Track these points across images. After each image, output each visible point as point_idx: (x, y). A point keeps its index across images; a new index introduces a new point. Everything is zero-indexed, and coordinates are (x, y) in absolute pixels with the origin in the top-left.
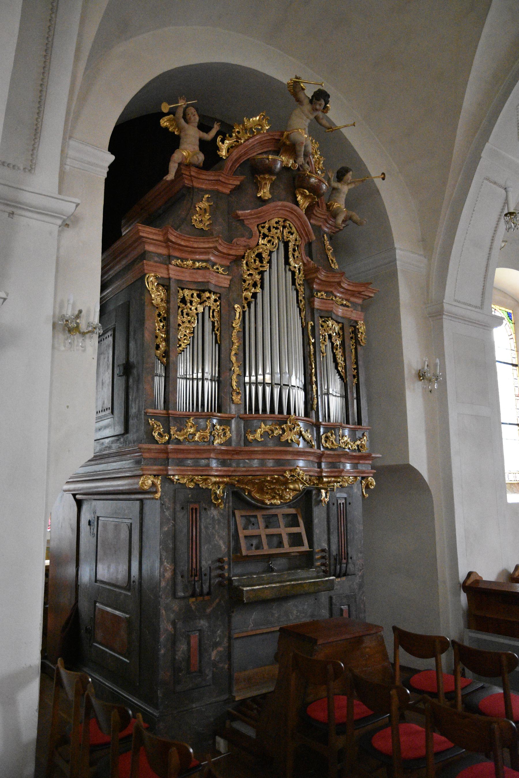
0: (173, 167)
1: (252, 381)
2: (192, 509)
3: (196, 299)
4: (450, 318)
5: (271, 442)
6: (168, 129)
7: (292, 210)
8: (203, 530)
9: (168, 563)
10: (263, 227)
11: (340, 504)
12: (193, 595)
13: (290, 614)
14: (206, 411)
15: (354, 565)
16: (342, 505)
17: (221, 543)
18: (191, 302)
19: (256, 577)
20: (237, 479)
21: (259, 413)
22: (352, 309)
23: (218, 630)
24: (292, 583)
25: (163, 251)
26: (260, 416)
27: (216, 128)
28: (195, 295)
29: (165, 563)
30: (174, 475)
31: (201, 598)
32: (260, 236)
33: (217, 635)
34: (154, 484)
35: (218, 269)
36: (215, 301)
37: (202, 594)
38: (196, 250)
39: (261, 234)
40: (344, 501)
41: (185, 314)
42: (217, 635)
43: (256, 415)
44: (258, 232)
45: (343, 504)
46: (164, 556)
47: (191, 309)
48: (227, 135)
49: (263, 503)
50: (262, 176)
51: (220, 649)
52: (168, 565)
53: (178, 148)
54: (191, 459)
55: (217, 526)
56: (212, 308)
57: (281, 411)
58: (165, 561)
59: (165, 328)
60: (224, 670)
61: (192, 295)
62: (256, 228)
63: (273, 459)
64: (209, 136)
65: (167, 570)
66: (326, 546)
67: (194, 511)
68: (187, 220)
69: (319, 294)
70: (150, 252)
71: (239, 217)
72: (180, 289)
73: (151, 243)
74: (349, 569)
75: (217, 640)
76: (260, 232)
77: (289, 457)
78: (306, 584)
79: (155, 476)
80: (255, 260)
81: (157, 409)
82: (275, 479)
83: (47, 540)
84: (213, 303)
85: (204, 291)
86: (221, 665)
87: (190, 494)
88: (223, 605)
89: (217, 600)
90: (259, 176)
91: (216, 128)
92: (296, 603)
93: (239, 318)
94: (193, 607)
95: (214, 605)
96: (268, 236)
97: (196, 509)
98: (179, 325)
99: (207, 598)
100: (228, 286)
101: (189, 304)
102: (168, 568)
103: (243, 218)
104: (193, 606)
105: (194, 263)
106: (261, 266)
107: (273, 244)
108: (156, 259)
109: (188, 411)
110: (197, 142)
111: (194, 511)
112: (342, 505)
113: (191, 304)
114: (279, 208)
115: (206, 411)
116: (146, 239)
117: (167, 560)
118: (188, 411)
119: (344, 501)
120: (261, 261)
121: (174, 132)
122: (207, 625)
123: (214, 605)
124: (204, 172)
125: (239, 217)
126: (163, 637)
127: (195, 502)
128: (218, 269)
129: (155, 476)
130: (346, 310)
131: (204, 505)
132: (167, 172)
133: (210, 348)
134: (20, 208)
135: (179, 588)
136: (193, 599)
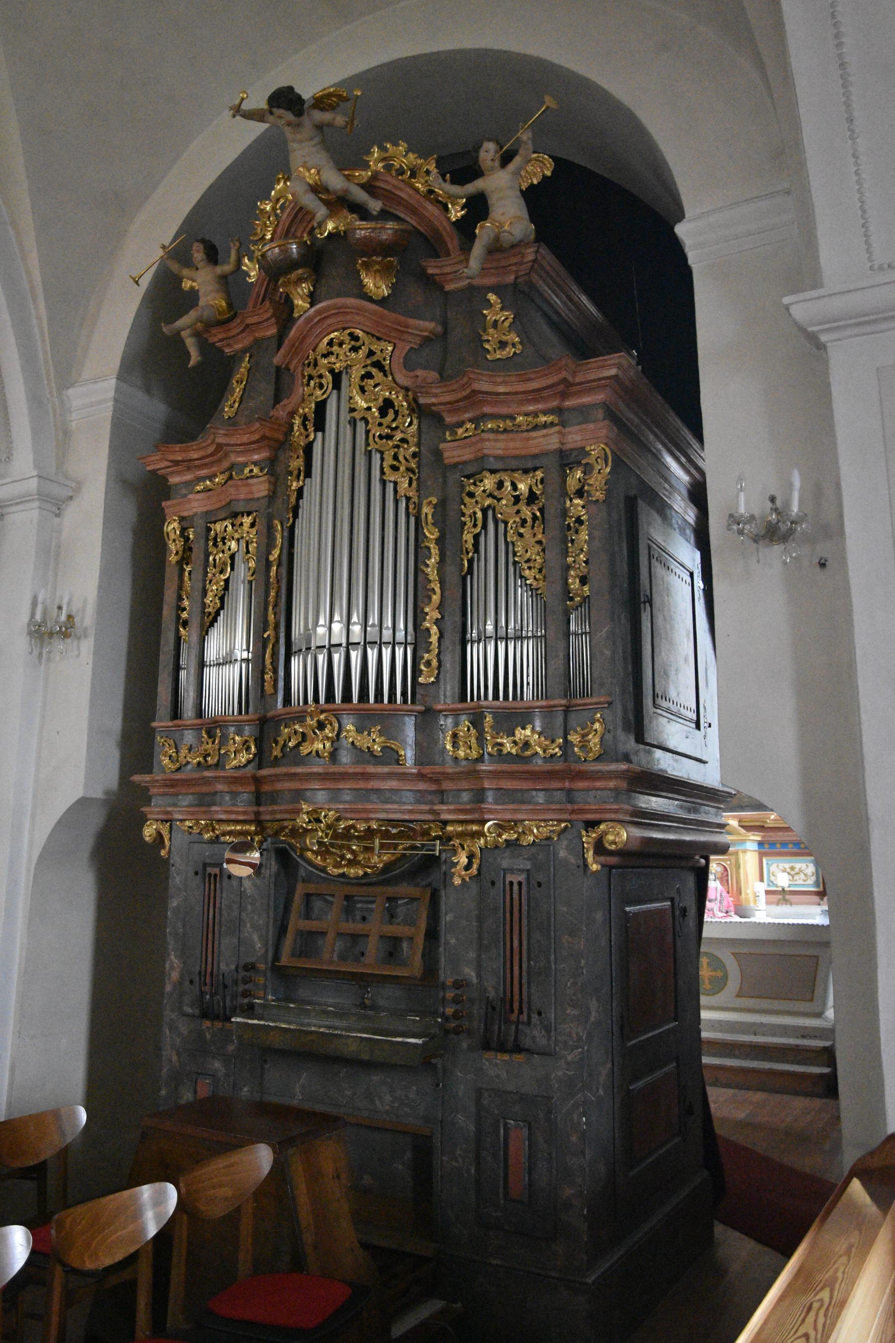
1: (384, 640)
4: (868, 329)
7: (340, 308)
8: (224, 913)
11: (511, 883)
15: (548, 1031)
16: (516, 887)
17: (256, 938)
19: (294, 1008)
21: (382, 701)
23: (245, 1086)
26: (385, 707)
29: (173, 957)
30: (182, 821)
34: (159, 835)
35: (251, 471)
36: (252, 525)
40: (522, 877)
45: (520, 884)
49: (323, 870)
57: (347, 696)
63: (193, 794)
66: (473, 974)
67: (212, 878)
69: (460, 431)
78: (351, 1040)
79: (162, 821)
81: (584, 696)
83: (767, 916)
84: (249, 530)
97: (216, 875)
102: (175, 965)
104: (207, 1035)
111: (212, 878)
112: (516, 887)
119: (522, 877)
122: (223, 1070)
128: (251, 471)
129: (162, 821)
130: (544, 436)
132: (189, 357)
134: (5, 506)
135: (187, 999)
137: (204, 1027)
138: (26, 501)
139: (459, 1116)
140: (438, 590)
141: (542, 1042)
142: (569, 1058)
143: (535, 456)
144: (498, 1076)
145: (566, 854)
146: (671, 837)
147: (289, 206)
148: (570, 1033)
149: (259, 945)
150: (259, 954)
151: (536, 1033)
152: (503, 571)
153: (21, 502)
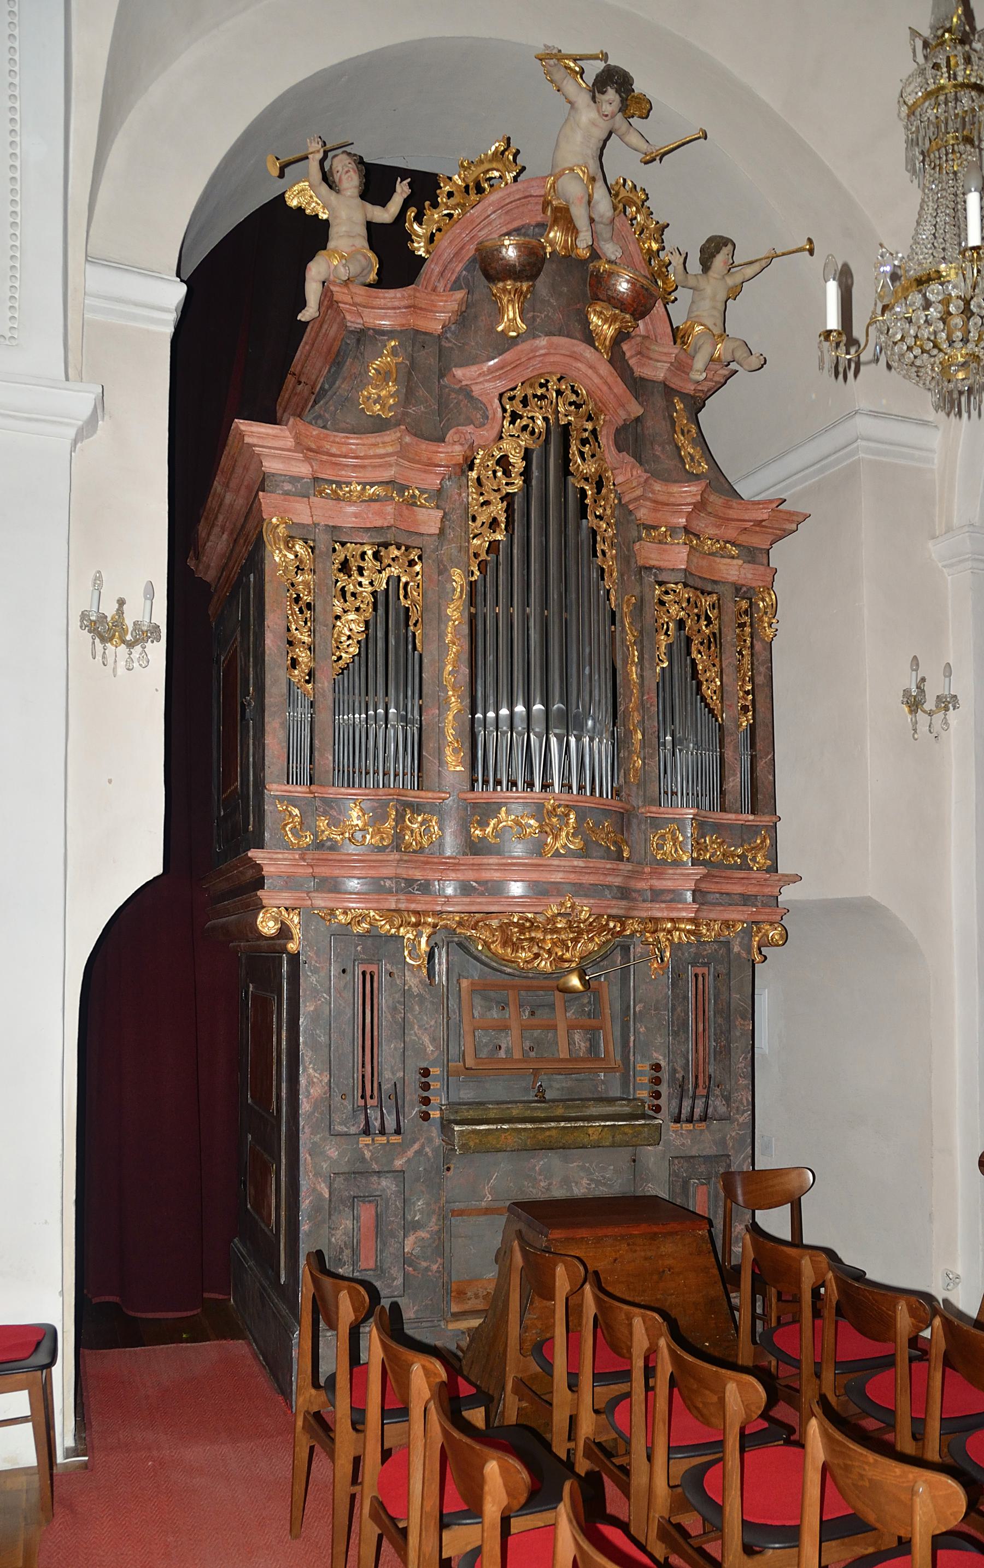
0: (313, 291)
2: (364, 973)
3: (369, 563)
5: (519, 846)
6: (304, 210)
9: (315, 1071)
10: (512, 399)
12: (367, 1131)
13: (573, 1184)
14: (605, 797)
17: (426, 1040)
18: (361, 571)
20: (457, 919)
22: (740, 562)
23: (418, 1200)
24: (562, 1124)
25: (303, 470)
27: (402, 190)
28: (370, 553)
29: (311, 1070)
31: (690, 1126)
32: (504, 418)
33: (417, 1208)
37: (690, 1120)
38: (338, 459)
39: (508, 414)
41: (348, 595)
42: (417, 1208)
43: (579, 798)
44: (500, 410)
46: (307, 1056)
47: (360, 584)
48: (427, 203)
50: (500, 285)
51: (423, 1234)
52: (316, 1075)
53: (325, 248)
54: (359, 878)
55: (417, 1008)
56: (404, 579)
58: (311, 1066)
59: (309, 624)
60: (430, 1273)
61: (363, 554)
62: (497, 401)
64: (385, 215)
65: (313, 1083)
67: (368, 977)
68: (349, 402)
70: (273, 475)
71: (461, 382)
72: (337, 546)
73: (274, 456)
74: (715, 1108)
75: (417, 1218)
76: (504, 410)
77: (496, 875)
80: (495, 472)
82: (527, 920)
85: (386, 545)
86: (424, 1264)
87: (359, 945)
88: (430, 1154)
89: (416, 1146)
90: (496, 285)
91: (402, 190)
92: (587, 1165)
93: (461, 597)
94: (368, 1155)
95: (410, 1153)
96: (521, 417)
98: (338, 618)
99: (395, 1139)
100: (437, 532)
101: (355, 573)
102: (315, 1080)
103: (468, 383)
105: (364, 489)
106: (507, 484)
107: (533, 433)
108: (287, 487)
109: (610, 797)
110: (364, 232)
113: (362, 575)
114: (542, 352)
115: (605, 797)
116: (260, 449)
117: (314, 1065)
118: (610, 797)
120: (507, 473)
121: (317, 215)
122: (394, 1188)
123: (410, 1153)
124: (381, 293)
125: (461, 382)
126: (307, 1201)
127: (370, 962)
131: (389, 967)
133: (608, 674)
136: (368, 1140)
137: (360, 1146)
138: (44, 421)
139: (650, 1185)
140: (445, 674)
141: (722, 1109)
142: (741, 1120)
143: (715, 582)
144: (683, 1145)
145: (739, 949)
146: (274, 1072)
147: (490, 205)
148: (742, 1099)
149: (432, 1048)
150: (432, 1058)
151: (718, 1103)
152: (402, 660)
153: (37, 420)
